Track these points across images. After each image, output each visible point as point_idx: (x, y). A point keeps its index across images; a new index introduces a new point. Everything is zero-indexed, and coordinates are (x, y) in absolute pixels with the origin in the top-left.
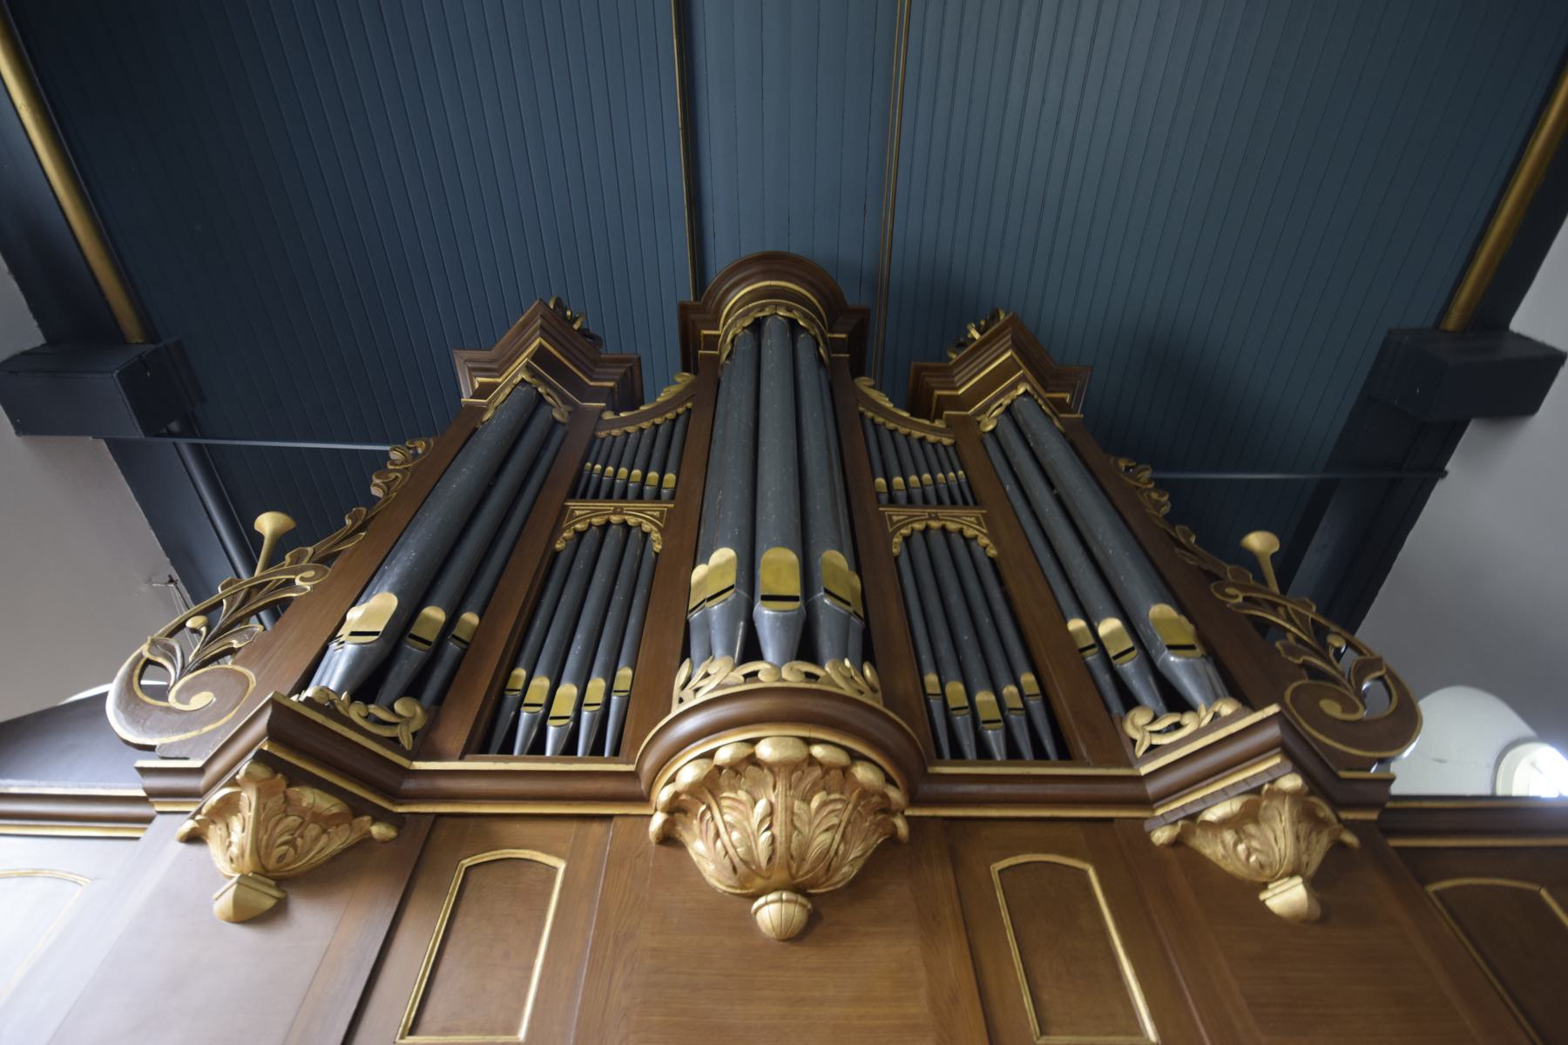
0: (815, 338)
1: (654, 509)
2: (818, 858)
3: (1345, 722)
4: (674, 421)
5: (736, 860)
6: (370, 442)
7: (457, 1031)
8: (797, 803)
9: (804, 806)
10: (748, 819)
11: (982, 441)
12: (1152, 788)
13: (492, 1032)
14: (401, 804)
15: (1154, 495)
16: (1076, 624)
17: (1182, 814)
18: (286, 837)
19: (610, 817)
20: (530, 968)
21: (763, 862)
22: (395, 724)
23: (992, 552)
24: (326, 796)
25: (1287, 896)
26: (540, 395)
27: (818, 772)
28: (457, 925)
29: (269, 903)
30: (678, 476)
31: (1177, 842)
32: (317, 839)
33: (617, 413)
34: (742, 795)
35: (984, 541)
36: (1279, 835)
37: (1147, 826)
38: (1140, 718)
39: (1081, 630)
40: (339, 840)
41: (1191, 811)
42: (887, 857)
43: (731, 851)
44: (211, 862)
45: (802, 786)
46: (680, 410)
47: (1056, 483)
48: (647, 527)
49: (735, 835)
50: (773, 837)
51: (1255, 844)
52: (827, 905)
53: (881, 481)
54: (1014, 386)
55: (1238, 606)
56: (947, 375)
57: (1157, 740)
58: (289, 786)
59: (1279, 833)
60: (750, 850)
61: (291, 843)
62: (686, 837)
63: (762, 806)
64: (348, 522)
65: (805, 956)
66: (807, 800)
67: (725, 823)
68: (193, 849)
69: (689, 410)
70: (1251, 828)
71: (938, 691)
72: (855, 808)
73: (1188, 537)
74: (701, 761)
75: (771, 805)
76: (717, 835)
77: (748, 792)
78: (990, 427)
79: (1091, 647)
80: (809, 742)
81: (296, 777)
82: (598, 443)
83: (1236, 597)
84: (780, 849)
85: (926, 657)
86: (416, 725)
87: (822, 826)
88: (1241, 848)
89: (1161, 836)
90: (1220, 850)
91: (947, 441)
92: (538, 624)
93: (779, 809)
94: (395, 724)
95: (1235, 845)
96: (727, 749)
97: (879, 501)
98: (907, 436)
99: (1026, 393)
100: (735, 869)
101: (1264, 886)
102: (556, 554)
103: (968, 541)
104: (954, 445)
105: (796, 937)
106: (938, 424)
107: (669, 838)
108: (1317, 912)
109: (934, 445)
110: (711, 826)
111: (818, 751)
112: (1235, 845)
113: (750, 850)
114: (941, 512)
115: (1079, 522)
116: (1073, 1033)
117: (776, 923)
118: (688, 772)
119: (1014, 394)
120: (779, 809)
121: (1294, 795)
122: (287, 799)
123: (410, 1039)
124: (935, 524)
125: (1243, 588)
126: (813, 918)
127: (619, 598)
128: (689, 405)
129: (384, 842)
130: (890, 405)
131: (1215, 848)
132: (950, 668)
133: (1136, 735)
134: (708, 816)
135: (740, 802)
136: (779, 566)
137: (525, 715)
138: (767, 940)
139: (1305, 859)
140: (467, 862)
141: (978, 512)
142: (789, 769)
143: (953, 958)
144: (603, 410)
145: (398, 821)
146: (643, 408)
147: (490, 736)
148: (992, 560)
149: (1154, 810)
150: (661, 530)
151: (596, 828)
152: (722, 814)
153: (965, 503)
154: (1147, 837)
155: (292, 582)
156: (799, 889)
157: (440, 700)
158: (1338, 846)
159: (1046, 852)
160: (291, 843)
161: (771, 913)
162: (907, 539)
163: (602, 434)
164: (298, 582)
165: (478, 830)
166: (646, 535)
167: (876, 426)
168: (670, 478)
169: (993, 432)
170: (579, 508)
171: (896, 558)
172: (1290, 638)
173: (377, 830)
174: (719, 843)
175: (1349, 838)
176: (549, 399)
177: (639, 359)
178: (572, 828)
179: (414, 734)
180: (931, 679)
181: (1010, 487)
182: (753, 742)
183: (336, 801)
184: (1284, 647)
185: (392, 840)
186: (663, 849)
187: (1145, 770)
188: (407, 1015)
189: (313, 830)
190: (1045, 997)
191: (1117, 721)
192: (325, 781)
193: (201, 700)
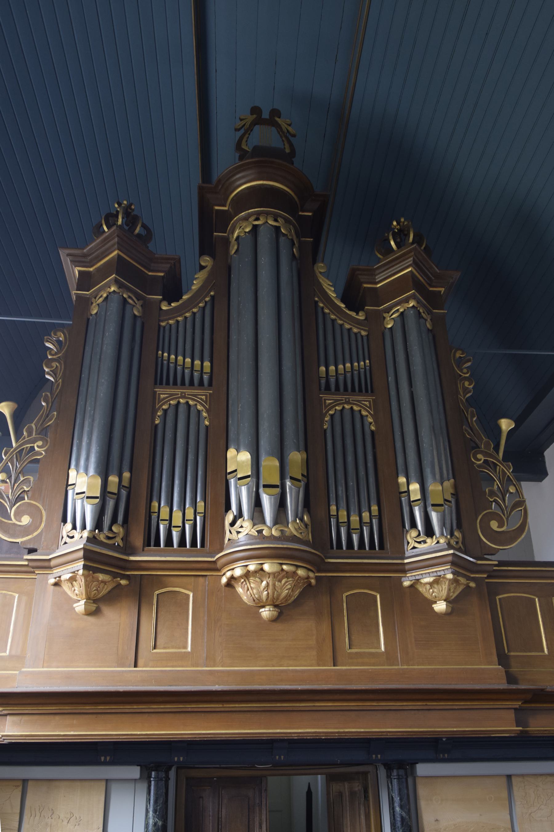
0: (292, 240)
1: (203, 394)
2: (283, 599)
3: (497, 531)
4: (204, 308)
5: (255, 599)
6: (21, 316)
7: (169, 648)
8: (276, 583)
9: (280, 584)
10: (259, 587)
11: (383, 334)
12: (407, 567)
13: (179, 648)
14: (127, 571)
15: (466, 384)
16: (402, 480)
17: (414, 578)
18: (95, 589)
19: (206, 576)
20: (187, 629)
21: (264, 600)
22: (115, 537)
23: (373, 428)
24: (106, 575)
25: (440, 607)
26: (125, 299)
27: (285, 573)
28: (159, 615)
29: (94, 609)
30: (211, 362)
31: (411, 586)
32: (103, 587)
33: (170, 304)
34: (257, 579)
35: (370, 420)
36: (443, 590)
37: (403, 579)
38: (414, 533)
39: (403, 483)
40: (109, 587)
41: (417, 578)
42: (307, 591)
43: (253, 596)
44: (65, 593)
45: (279, 577)
46: (207, 299)
47: (413, 387)
48: (199, 407)
49: (255, 591)
50: (268, 593)
51: (435, 590)
52: (284, 610)
53: (323, 369)
54: (407, 300)
55: (479, 466)
56: (371, 274)
57: (417, 545)
58: (94, 573)
59: (444, 589)
60: (260, 597)
61: (97, 590)
62: (236, 585)
63: (264, 583)
64: (44, 404)
65: (278, 626)
66: (280, 581)
67: (251, 587)
68: (57, 588)
69: (213, 297)
70: (436, 586)
71: (335, 514)
72: (297, 581)
73: (473, 417)
74: (242, 567)
75: (268, 583)
76: (248, 589)
77: (259, 578)
78: (389, 326)
79: (405, 492)
80: (281, 564)
81: (96, 570)
82: (162, 329)
83: (480, 460)
84: (270, 597)
85: (333, 495)
86: (121, 535)
87: (285, 589)
88: (431, 590)
89: (406, 583)
90: (424, 590)
91: (364, 333)
92: (157, 474)
93: (271, 584)
94: (115, 537)
95: (429, 589)
96: (252, 566)
97: (320, 390)
98: (341, 326)
99: (413, 306)
100: (254, 600)
101: (435, 602)
102: (156, 426)
103: (362, 416)
104: (367, 336)
105: (275, 620)
106: (361, 316)
107: (229, 584)
108: (450, 610)
109: (356, 334)
110: (246, 586)
111: (285, 567)
112: (429, 589)
113: (260, 597)
114: (352, 398)
115: (417, 417)
116: (359, 649)
117: (268, 617)
118: (238, 572)
119: (406, 305)
120: (271, 584)
121: (450, 580)
122: (93, 577)
123: (155, 651)
124: (347, 407)
125: (485, 454)
126: (280, 614)
127: (191, 457)
128: (212, 293)
129: (126, 586)
130: (333, 295)
131: (421, 589)
132: (343, 504)
133: (410, 540)
134: (245, 583)
135: (257, 581)
136: (269, 464)
137: (162, 527)
138: (265, 621)
139: (451, 594)
140: (157, 592)
141: (370, 398)
142: (274, 575)
143: (325, 628)
144: (161, 301)
145: (127, 577)
146: (185, 297)
147: (151, 540)
148: (372, 432)
149: (406, 574)
150: (208, 411)
151: (201, 580)
152: (250, 584)
153: (367, 391)
154: (401, 583)
155: (32, 448)
156: (275, 606)
157: (126, 521)
158: (468, 587)
159: (364, 589)
160: (97, 590)
161: (266, 613)
162: (332, 416)
163: (163, 324)
164: (36, 448)
165: (159, 582)
166: (199, 412)
167: (324, 314)
168: (207, 364)
169: (391, 328)
170: (163, 393)
171: (325, 431)
172: (496, 487)
173: (123, 582)
174: (248, 592)
175: (472, 585)
176: (130, 301)
177: (180, 259)
178: (193, 579)
179: (122, 539)
180: (333, 508)
181: (391, 379)
182: (262, 564)
183: (109, 576)
184: (490, 491)
185: (128, 585)
186: (227, 588)
187: (406, 561)
188: (152, 643)
189: (102, 585)
190: (353, 638)
191: (405, 533)
192: (104, 570)
193: (26, 520)
